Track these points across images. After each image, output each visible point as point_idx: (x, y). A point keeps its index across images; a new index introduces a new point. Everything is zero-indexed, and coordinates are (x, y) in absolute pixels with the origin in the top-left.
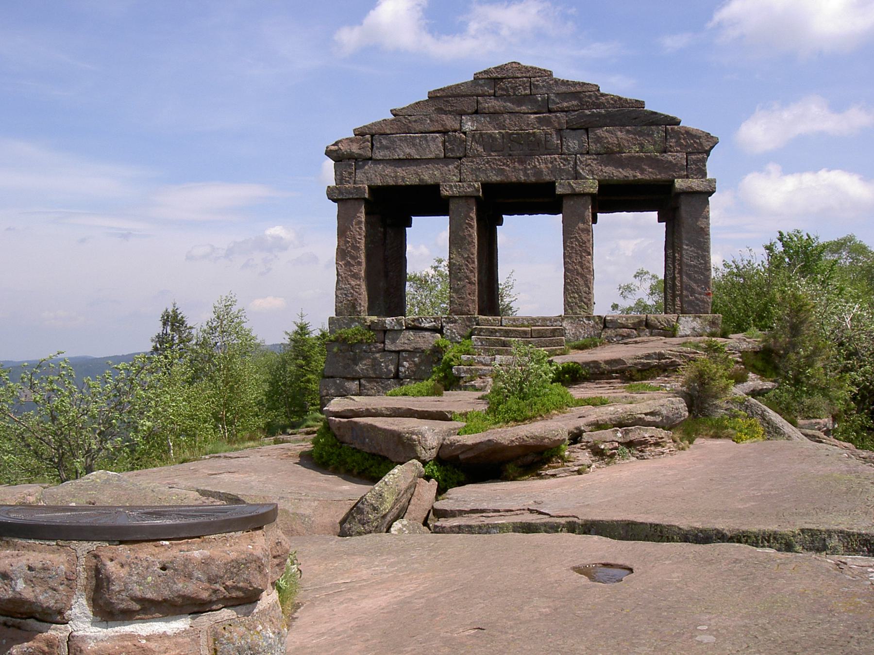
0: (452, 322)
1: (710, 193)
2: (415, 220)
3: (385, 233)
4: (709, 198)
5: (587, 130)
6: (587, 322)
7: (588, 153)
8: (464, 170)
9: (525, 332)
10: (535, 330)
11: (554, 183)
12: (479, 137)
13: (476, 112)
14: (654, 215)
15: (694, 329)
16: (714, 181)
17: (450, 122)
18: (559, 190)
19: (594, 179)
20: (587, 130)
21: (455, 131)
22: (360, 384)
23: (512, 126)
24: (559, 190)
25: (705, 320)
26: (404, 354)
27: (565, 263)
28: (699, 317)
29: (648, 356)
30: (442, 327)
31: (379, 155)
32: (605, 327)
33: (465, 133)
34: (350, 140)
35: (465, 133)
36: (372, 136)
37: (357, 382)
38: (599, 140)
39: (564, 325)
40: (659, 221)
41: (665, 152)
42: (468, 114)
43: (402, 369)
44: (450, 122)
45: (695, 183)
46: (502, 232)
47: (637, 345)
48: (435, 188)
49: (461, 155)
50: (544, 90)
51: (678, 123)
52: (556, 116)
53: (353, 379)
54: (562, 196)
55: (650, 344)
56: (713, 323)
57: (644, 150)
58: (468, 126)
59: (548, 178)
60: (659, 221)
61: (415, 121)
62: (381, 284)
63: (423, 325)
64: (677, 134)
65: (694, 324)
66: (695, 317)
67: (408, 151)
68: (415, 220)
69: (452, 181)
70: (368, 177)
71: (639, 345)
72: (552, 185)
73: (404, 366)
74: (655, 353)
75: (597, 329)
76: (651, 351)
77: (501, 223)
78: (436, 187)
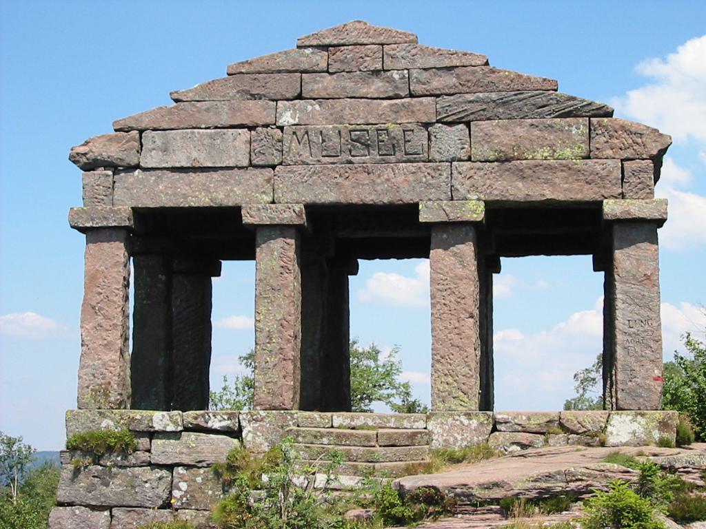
0: (256, 420)
1: (660, 222)
2: (226, 265)
3: (169, 285)
4: (659, 230)
5: (468, 124)
6: (466, 422)
7: (469, 159)
8: (279, 185)
9: (367, 438)
10: (383, 434)
11: (417, 205)
12: (301, 131)
13: (300, 97)
14: (589, 258)
15: (634, 433)
16: (665, 202)
17: (256, 111)
18: (423, 218)
19: (479, 199)
20: (468, 124)
21: (266, 126)
22: (112, 516)
23: (358, 114)
24: (423, 218)
25: (653, 420)
26: (181, 470)
27: (433, 330)
28: (642, 415)
29: (549, 476)
30: (240, 429)
31: (149, 160)
32: (494, 429)
33: (281, 128)
34: (111, 139)
35: (281, 128)
36: (141, 132)
37: (107, 513)
38: (488, 138)
39: (430, 427)
40: (595, 269)
41: (588, 157)
42: (288, 100)
43: (176, 493)
44: (256, 111)
45: (635, 207)
46: (499, 282)
47: (539, 459)
48: (234, 212)
49: (276, 162)
50: (402, 64)
51: (609, 114)
52: (421, 103)
53: (101, 508)
54: (430, 226)
55: (561, 458)
56: (664, 425)
57: (556, 155)
58: (287, 119)
59: (408, 198)
60: (595, 269)
61: (208, 110)
62: (161, 361)
63: (210, 425)
64: (612, 133)
65: (635, 426)
66: (637, 415)
67: (195, 154)
68: (226, 265)
69: (260, 200)
70: (652, 195)
71: (543, 459)
72: (413, 208)
73: (180, 489)
74: (559, 473)
75: (481, 434)
76: (552, 470)
77: (355, 271)
78: (236, 211)
